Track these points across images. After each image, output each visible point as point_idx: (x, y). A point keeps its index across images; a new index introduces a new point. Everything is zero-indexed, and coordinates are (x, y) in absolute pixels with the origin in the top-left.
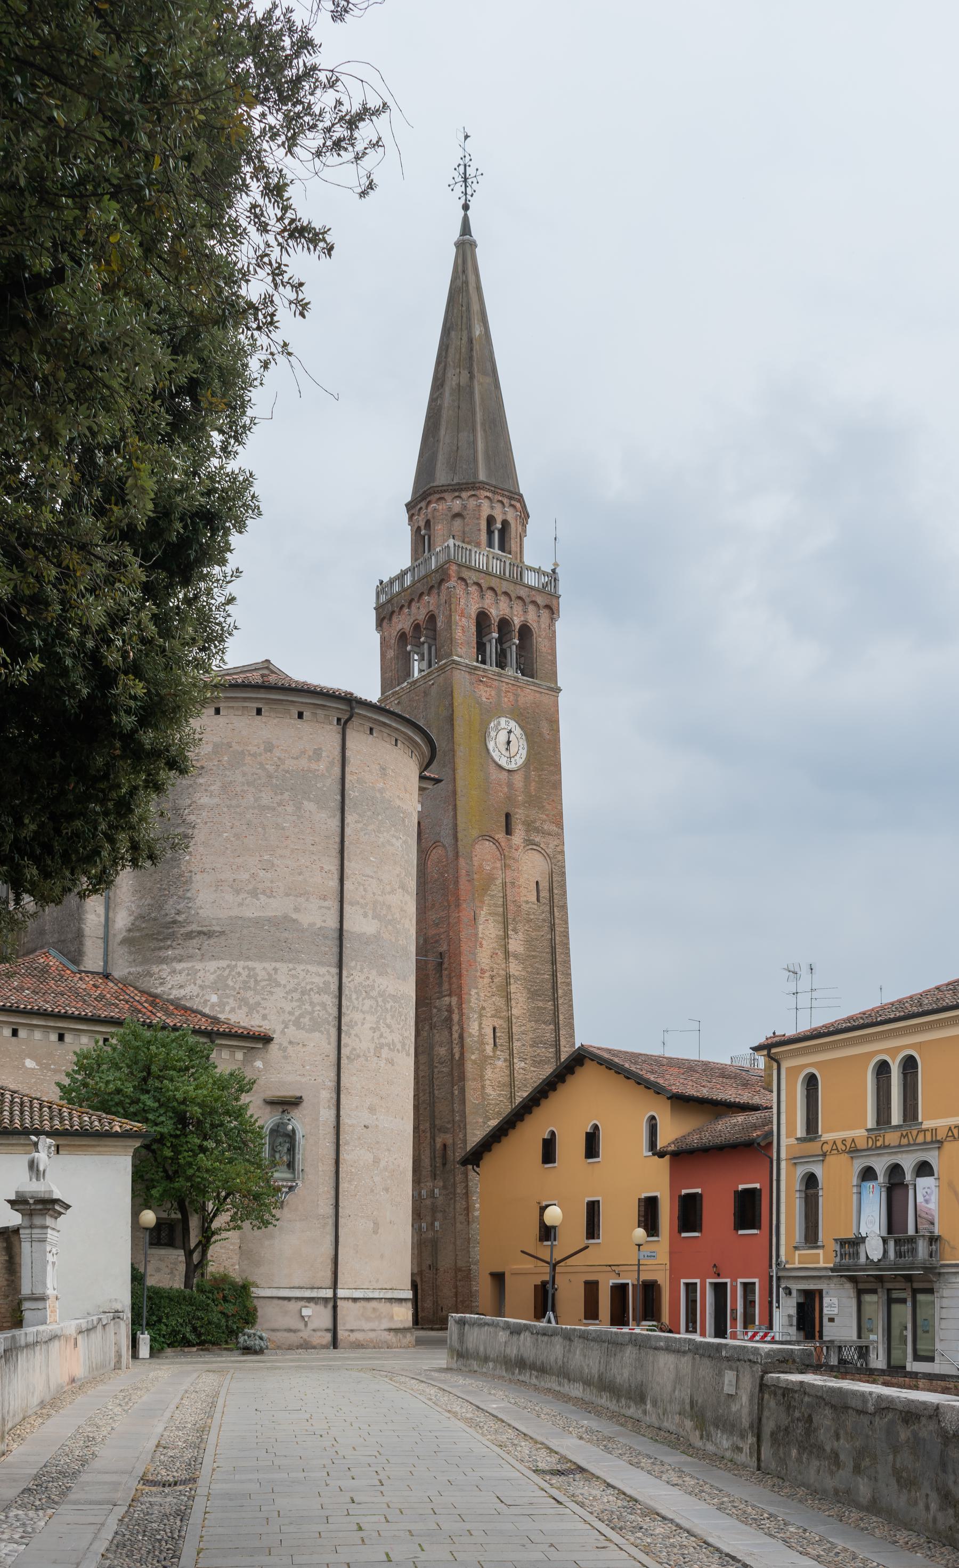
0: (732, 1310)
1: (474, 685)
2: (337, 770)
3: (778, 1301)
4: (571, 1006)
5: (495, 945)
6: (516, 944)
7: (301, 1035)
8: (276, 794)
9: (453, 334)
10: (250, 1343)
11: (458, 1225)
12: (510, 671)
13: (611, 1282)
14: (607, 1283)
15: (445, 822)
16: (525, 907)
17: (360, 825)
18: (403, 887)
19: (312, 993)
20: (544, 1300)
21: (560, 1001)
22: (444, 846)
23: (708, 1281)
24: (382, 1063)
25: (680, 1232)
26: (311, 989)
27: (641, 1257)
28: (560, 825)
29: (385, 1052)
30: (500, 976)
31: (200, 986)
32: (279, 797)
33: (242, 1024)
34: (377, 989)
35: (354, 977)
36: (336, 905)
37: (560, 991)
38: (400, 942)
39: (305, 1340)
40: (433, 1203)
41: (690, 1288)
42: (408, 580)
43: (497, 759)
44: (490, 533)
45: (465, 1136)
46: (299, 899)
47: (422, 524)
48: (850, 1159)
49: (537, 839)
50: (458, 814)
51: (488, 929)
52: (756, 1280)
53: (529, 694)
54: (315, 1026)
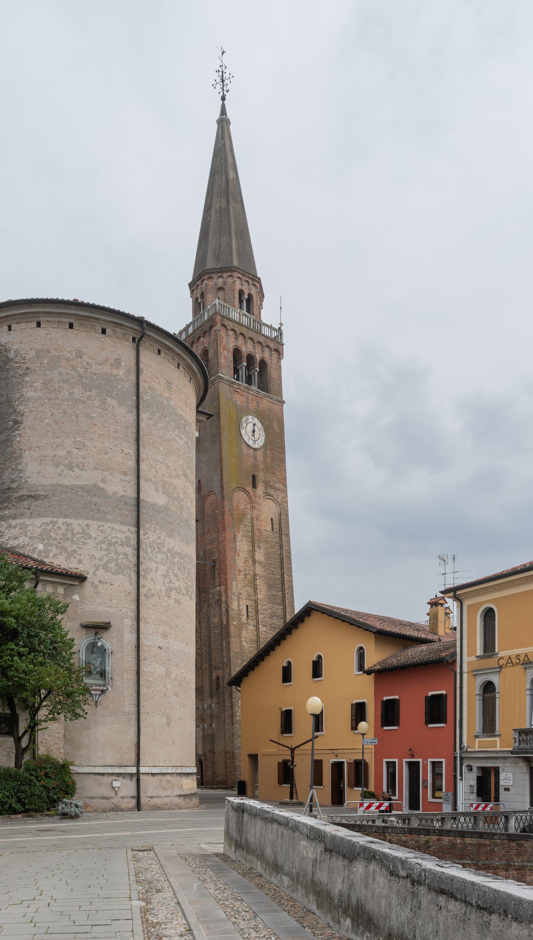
0: (423, 781)
1: (231, 393)
2: (133, 377)
3: (461, 775)
4: (293, 595)
5: (247, 555)
6: (260, 556)
7: (108, 576)
8: (85, 390)
9: (216, 176)
10: (67, 810)
11: (226, 725)
12: (254, 388)
13: (332, 761)
14: (328, 762)
15: (215, 478)
16: (264, 533)
17: (151, 422)
18: (185, 475)
19: (116, 545)
20: (286, 773)
21: (286, 592)
22: (215, 494)
23: (404, 760)
24: (172, 602)
25: (382, 726)
26: (116, 542)
27: (365, 743)
28: (285, 485)
29: (173, 594)
30: (250, 574)
31: (30, 537)
32: (88, 393)
33: (63, 566)
34: (167, 547)
35: (149, 537)
36: (134, 480)
37: (286, 586)
38: (184, 515)
39: (116, 805)
40: (211, 713)
41: (391, 765)
42: (191, 330)
43: (247, 441)
44: (241, 301)
45: (230, 671)
46: (105, 473)
47: (199, 295)
48: (523, 670)
49: (272, 493)
50: (224, 473)
51: (242, 546)
52: (443, 760)
53: (265, 403)
54: (120, 571)
